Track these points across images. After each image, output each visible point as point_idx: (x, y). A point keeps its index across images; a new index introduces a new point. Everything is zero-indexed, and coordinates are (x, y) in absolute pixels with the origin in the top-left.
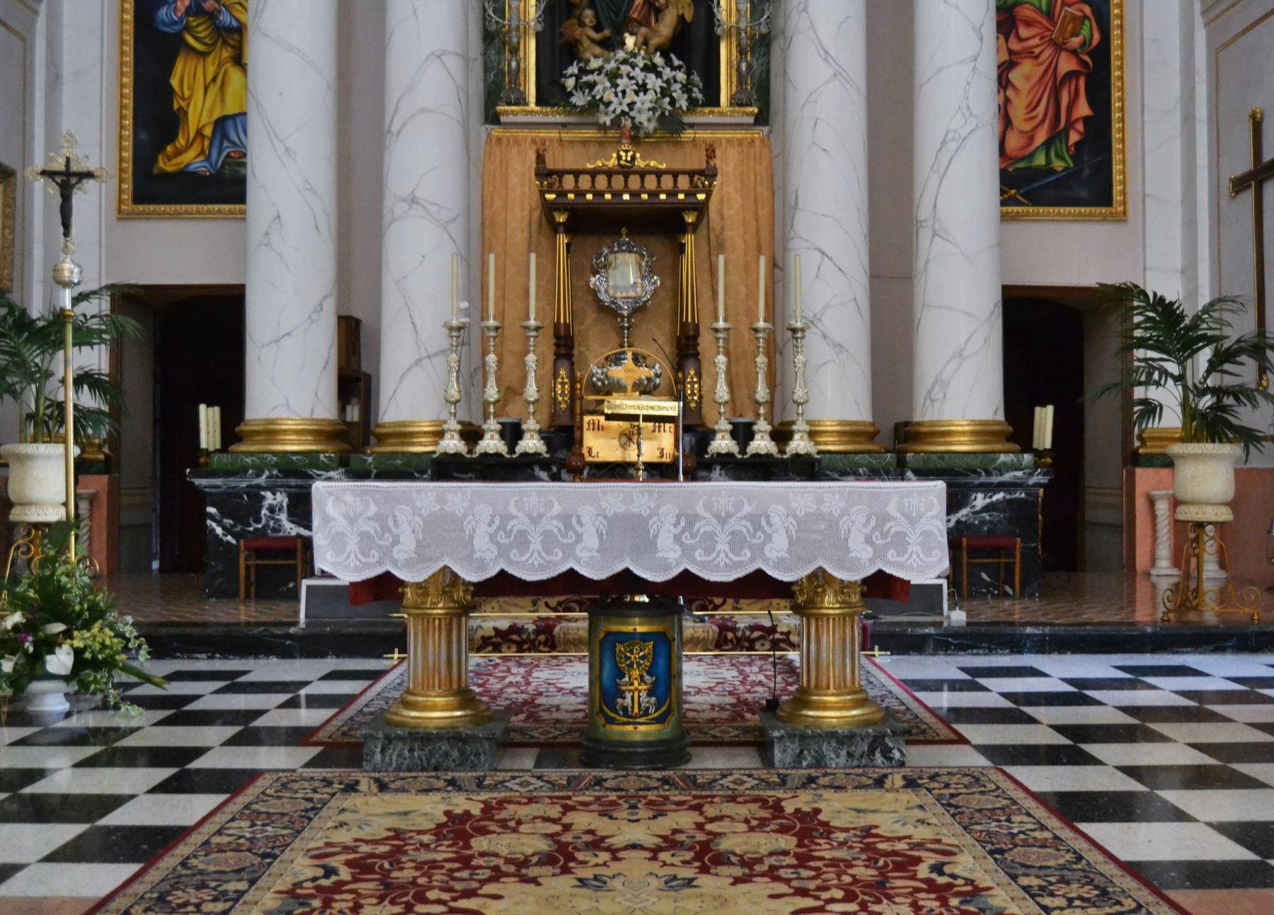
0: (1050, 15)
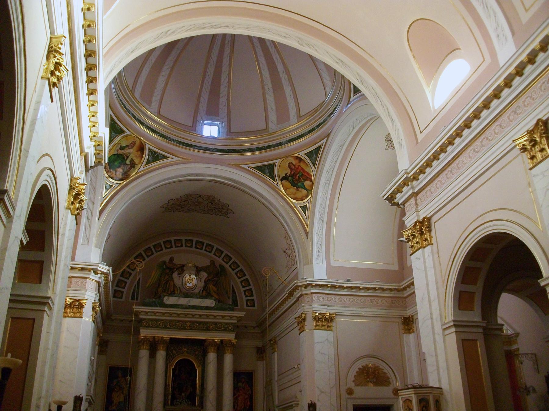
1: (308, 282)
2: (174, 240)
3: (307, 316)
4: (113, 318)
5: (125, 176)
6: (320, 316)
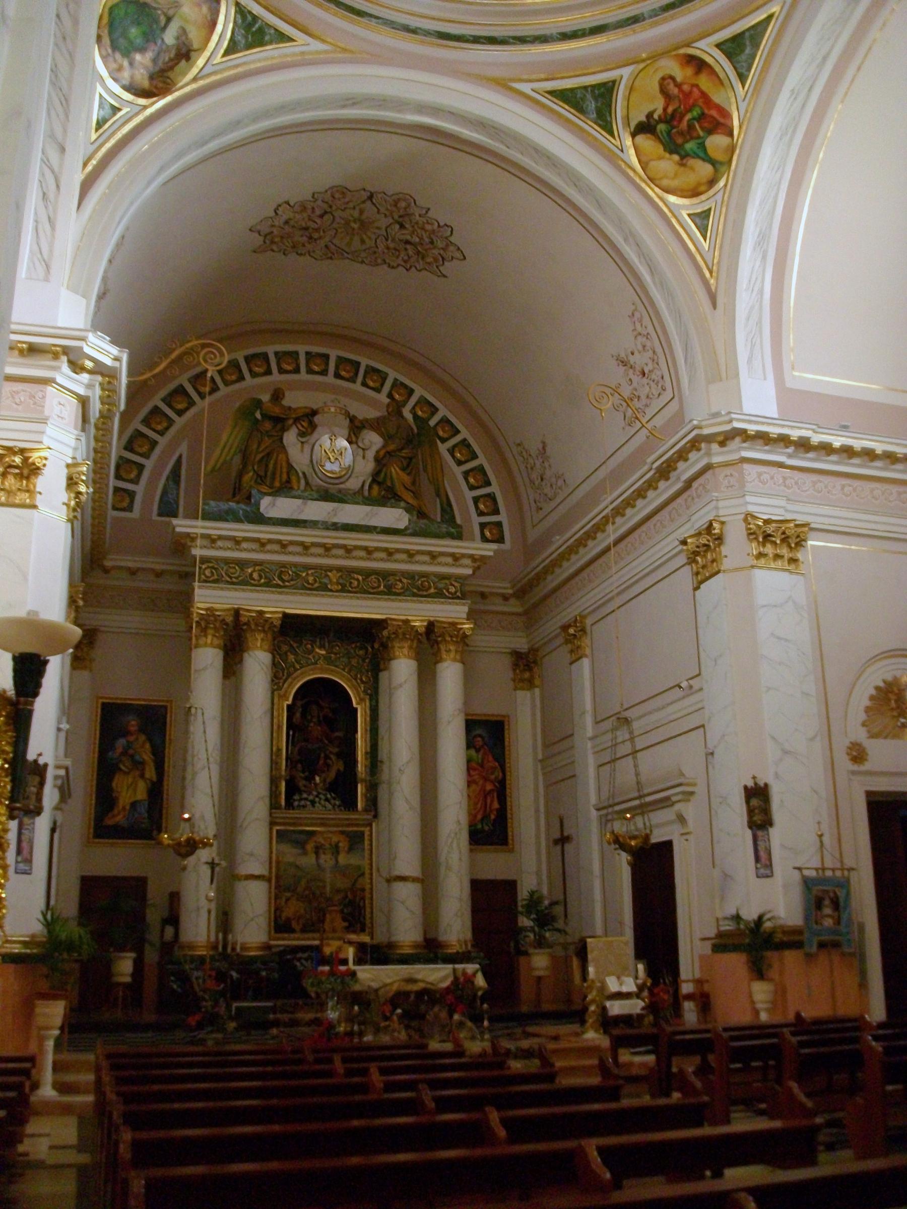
0: (482, 766)
3: (727, 528)
4: (108, 563)
5: (158, 84)
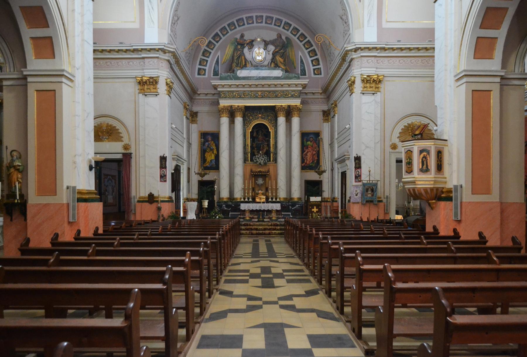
1: (357, 46)
2: (246, 17)
4: (198, 92)
6: (368, 78)
